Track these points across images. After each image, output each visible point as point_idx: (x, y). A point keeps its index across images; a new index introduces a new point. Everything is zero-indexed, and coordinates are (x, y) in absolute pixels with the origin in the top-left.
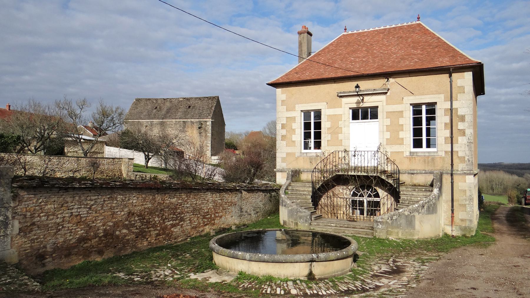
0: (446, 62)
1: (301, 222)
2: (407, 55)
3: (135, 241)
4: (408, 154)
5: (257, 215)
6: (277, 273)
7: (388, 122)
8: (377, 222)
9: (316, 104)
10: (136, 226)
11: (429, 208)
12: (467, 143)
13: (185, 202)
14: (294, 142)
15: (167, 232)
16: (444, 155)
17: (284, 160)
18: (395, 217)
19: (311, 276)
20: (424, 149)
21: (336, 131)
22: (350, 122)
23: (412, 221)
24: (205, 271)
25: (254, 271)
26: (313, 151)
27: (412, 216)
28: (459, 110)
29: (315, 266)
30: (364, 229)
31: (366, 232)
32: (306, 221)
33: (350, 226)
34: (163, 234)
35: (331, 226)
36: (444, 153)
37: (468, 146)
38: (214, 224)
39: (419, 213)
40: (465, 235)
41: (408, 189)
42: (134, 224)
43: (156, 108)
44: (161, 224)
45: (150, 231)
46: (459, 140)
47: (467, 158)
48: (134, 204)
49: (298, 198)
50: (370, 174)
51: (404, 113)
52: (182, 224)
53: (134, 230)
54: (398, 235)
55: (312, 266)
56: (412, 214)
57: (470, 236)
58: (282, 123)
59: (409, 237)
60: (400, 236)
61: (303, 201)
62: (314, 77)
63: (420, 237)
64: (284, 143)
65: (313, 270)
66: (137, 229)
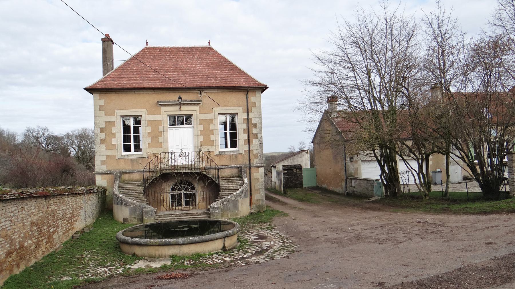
0: (242, 83)
2: (211, 74)
4: (218, 153)
6: (204, 250)
7: (201, 127)
8: (214, 208)
9: (136, 110)
11: (245, 193)
14: (114, 145)
17: (103, 162)
20: (133, 152)
25: (185, 252)
26: (229, 149)
30: (200, 215)
33: (188, 215)
37: (259, 146)
41: (224, 181)
47: (259, 154)
50: (193, 171)
51: (214, 120)
54: (228, 216)
56: (237, 199)
57: (263, 211)
61: (138, 198)
62: (134, 86)
64: (104, 146)
65: (225, 244)
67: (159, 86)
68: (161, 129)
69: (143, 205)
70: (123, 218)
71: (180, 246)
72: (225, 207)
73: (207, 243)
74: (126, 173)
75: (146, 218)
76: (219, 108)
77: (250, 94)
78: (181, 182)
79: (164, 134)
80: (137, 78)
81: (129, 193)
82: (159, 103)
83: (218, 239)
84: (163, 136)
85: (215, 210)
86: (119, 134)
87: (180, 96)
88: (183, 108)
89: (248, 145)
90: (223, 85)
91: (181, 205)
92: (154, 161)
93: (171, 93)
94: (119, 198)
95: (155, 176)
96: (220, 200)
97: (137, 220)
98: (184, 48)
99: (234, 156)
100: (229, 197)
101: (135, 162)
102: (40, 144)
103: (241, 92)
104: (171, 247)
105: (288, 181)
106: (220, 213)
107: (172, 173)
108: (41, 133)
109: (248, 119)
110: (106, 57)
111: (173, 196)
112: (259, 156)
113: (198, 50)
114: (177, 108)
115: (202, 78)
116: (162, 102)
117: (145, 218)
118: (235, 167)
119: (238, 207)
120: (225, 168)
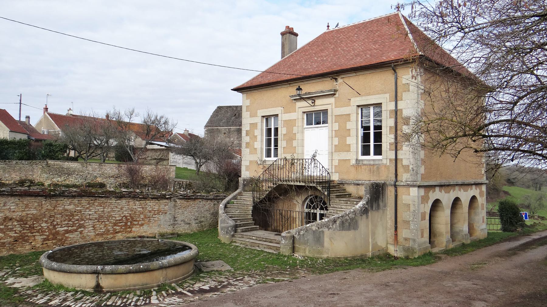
3: (13, 244)
4: (353, 162)
6: (67, 283)
7: (336, 126)
10: (15, 231)
11: (343, 223)
13: (86, 209)
15: (59, 237)
17: (247, 168)
18: (303, 232)
19: (98, 289)
21: (291, 138)
22: (304, 127)
23: (320, 237)
27: (320, 232)
29: (102, 279)
32: (227, 232)
33: (267, 240)
34: (53, 239)
35: (253, 239)
36: (388, 161)
37: (412, 152)
38: (130, 232)
40: (408, 256)
41: (341, 201)
42: (13, 228)
43: (236, 115)
44: (50, 230)
45: (34, 236)
47: (411, 167)
48: (12, 210)
49: (240, 208)
52: (82, 231)
53: (12, 234)
54: (305, 252)
55: (100, 278)
56: (320, 230)
58: (247, 129)
61: (242, 211)
63: (329, 256)
64: (248, 150)
65: (100, 282)
66: (16, 233)
68: (295, 130)
73: (70, 275)
76: (358, 99)
77: (400, 71)
93: (306, 85)
112: (410, 169)
119: (323, 243)
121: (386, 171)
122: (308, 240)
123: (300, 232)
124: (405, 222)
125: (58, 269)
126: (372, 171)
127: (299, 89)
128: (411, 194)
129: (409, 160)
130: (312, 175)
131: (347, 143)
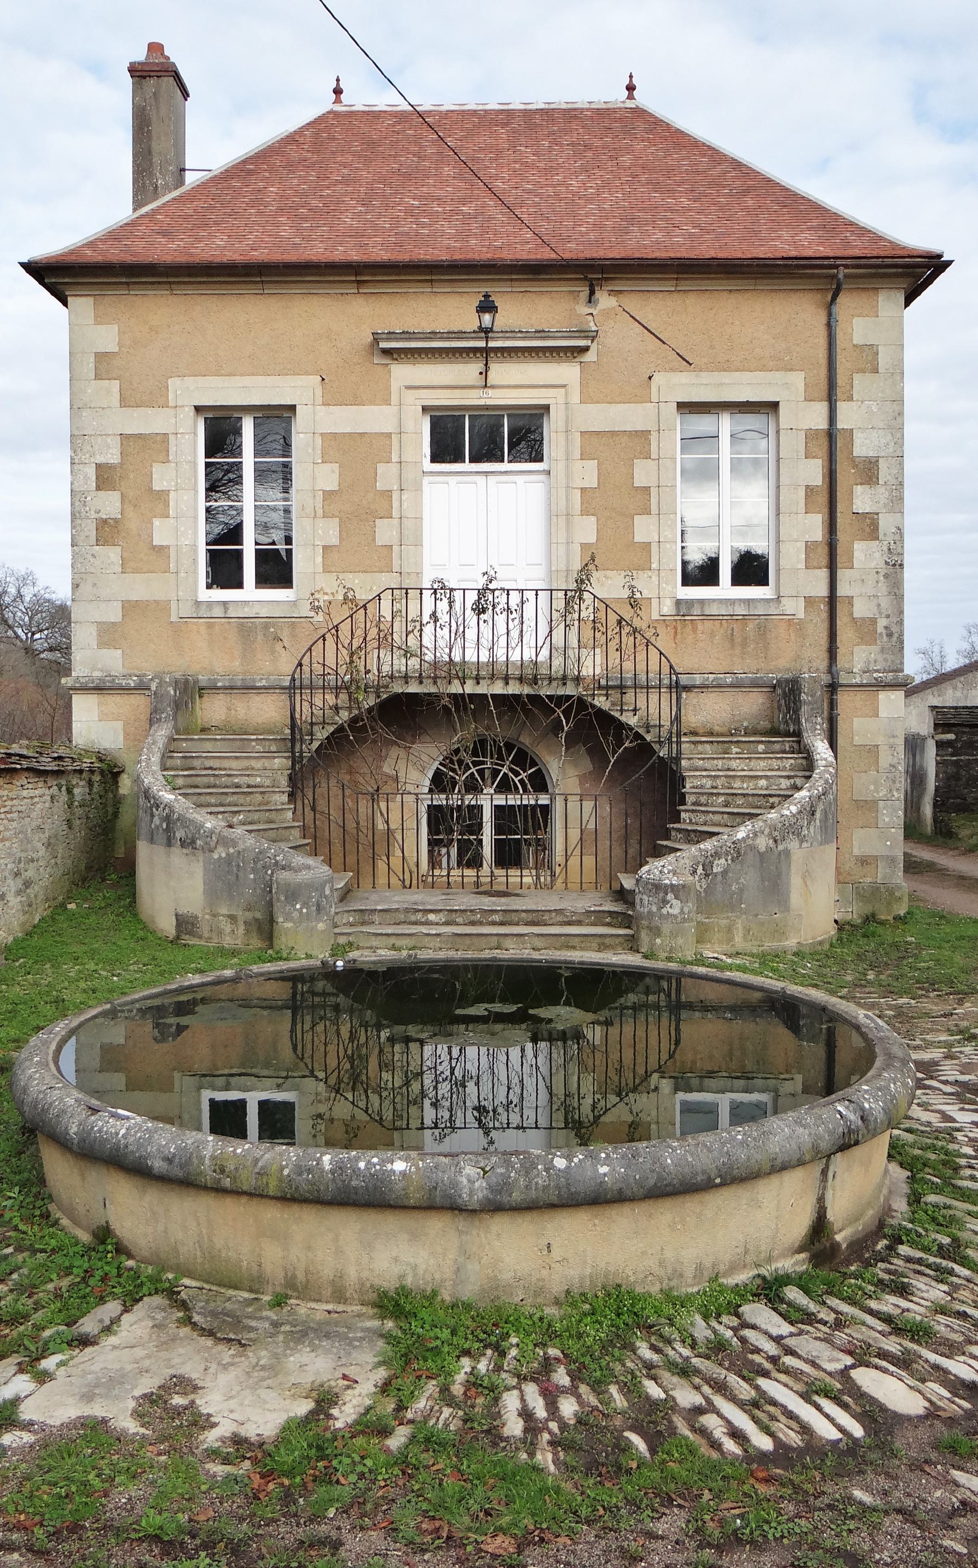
1: (296, 915)
2: (643, 210)
4: (668, 608)
5: (28, 896)
7: (588, 474)
8: (658, 888)
12: (883, 565)
14: (162, 550)
16: (801, 615)
18: (723, 861)
23: (779, 876)
24: (88, 1325)
25: (506, 1276)
27: (780, 854)
28: (858, 438)
30: (579, 923)
31: (601, 936)
32: (319, 908)
33: (515, 918)
37: (886, 576)
39: (802, 842)
40: (873, 915)
41: (700, 747)
46: (856, 554)
47: (882, 623)
50: (545, 691)
51: (653, 438)
54: (730, 940)
56: (781, 848)
57: (890, 918)
58: (100, 459)
59: (770, 945)
60: (739, 942)
61: (256, 816)
62: (260, 255)
64: (113, 554)
65: (828, 1204)
67: (380, 254)
68: (386, 476)
69: (281, 852)
70: (177, 915)
71: (462, 1222)
72: (719, 888)
73: (691, 1204)
74: (214, 688)
75: (286, 920)
78: (480, 747)
79: (405, 505)
80: (277, 224)
81: (214, 786)
82: (383, 345)
83: (780, 1167)
84: (395, 513)
85: (665, 902)
86: (186, 496)
87: (487, 296)
88: (501, 372)
89: (824, 574)
90: (707, 250)
91: (476, 862)
92: (345, 628)
94: (158, 807)
95: (350, 709)
96: (694, 849)
97: (241, 930)
98: (510, 113)
99: (751, 626)
100: (741, 834)
101: (260, 637)
102: (10, 627)
103: (801, 294)
104: (390, 1222)
105: (956, 777)
106: (690, 920)
107: (438, 697)
108: (12, 590)
109: (831, 434)
110: (150, 152)
111: (437, 817)
112: (880, 629)
113: (576, 117)
114: (469, 371)
115: (598, 227)
116: (397, 340)
117: (284, 924)
118: (755, 684)
119: (788, 896)
120: (704, 687)
121: (793, 638)
122: (741, 890)
123: (711, 863)
124: (862, 803)
125: (639, 1183)
126: (738, 640)
127: (487, 306)
128: (883, 713)
129: (875, 601)
130: (457, 658)
131: (637, 539)
